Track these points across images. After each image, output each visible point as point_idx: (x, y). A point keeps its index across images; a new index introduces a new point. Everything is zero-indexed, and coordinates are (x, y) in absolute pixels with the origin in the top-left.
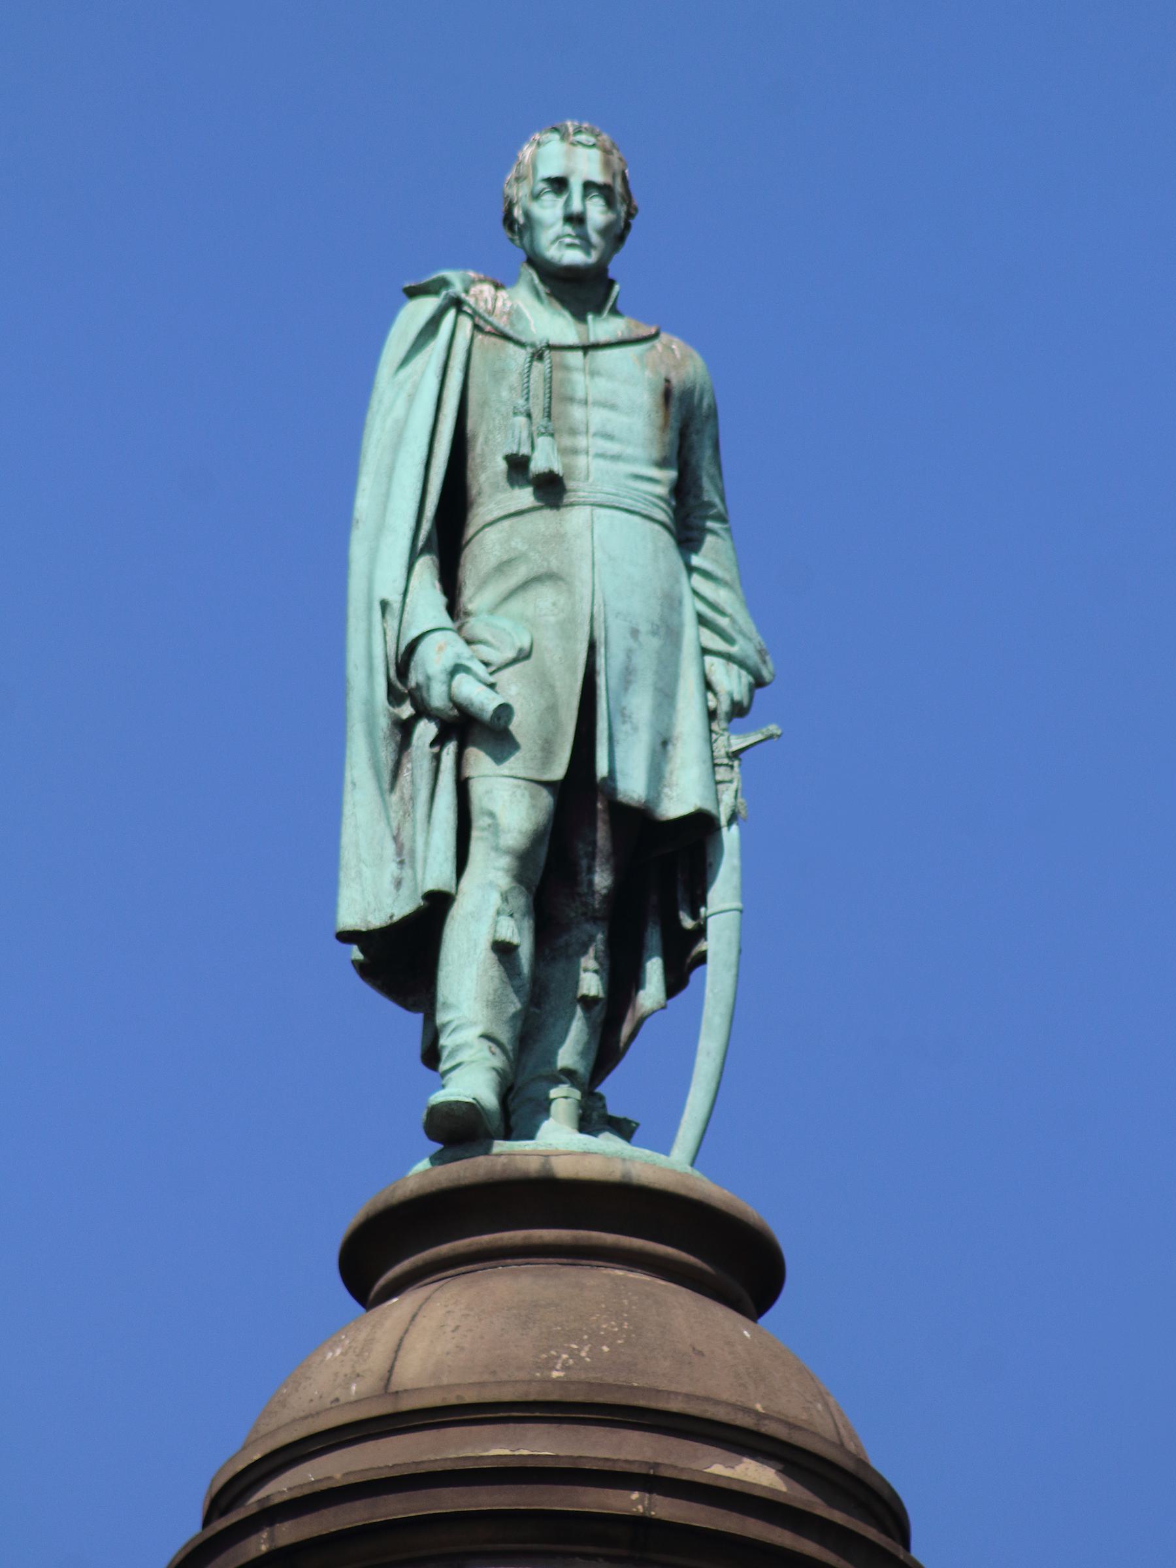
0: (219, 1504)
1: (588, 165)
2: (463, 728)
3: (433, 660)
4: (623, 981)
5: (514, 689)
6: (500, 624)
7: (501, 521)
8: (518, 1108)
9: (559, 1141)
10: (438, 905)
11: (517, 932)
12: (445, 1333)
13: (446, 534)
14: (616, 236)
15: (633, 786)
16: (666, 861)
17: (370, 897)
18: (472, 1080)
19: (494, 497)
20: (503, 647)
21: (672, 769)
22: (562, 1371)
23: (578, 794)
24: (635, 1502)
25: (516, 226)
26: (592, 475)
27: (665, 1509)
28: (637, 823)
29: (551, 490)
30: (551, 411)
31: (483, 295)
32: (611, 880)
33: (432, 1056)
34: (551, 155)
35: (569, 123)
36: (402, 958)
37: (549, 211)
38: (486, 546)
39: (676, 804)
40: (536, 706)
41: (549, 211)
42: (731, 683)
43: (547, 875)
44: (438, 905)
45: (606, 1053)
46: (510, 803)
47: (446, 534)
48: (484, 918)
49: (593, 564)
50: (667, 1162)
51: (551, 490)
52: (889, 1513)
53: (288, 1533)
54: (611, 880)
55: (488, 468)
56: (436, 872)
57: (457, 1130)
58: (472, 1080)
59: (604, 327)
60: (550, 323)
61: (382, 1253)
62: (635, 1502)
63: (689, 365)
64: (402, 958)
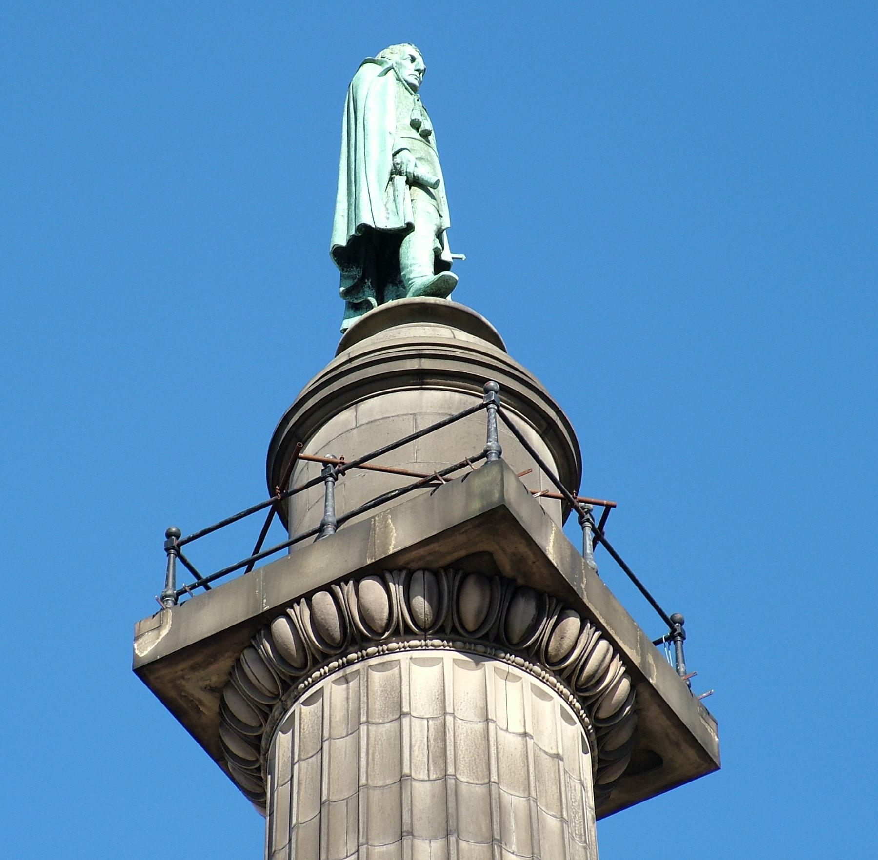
10: (410, 228)
44: (410, 228)
61: (344, 346)
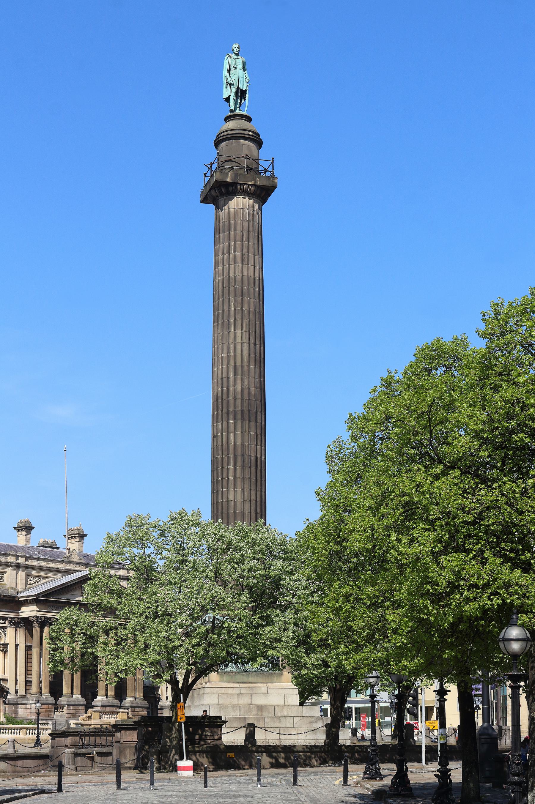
0: (217, 136)
1: (237, 46)
2: (231, 84)
3: (229, 80)
4: (241, 101)
5: (234, 82)
6: (233, 78)
7: (233, 71)
8: (235, 110)
9: (238, 112)
10: (230, 96)
11: (235, 98)
12: (231, 124)
13: (229, 71)
14: (239, 51)
15: (241, 88)
16: (244, 92)
17: (225, 96)
18: (232, 108)
19: (232, 69)
20: (233, 79)
21: (243, 87)
22: (239, 127)
23: (238, 88)
24: (244, 135)
25: (233, 50)
26: (238, 67)
27: (245, 136)
28: (242, 90)
29: (236, 68)
30: (236, 63)
31: (231, 55)
32: (241, 94)
33: (229, 106)
34: (235, 46)
35: (511, 452)
36: (227, 100)
37: (235, 49)
38: (232, 72)
39: (244, 89)
40: (235, 83)
41: (235, 49)
42: (247, 81)
43: (236, 94)
44: (230, 96)
45: (240, 106)
46: (234, 89)
47: (229, 71)
48: (233, 97)
49: (16, 681)
50: (244, 113)
51: (236, 68)
52: (259, 136)
53: (222, 138)
54: (241, 94)
55: (232, 67)
56: (230, 94)
57: (231, 111)
58: (232, 108)
59: (239, 57)
60: (235, 57)
61: (227, 119)
62: (244, 135)
63: (244, 60)
64: (227, 100)
